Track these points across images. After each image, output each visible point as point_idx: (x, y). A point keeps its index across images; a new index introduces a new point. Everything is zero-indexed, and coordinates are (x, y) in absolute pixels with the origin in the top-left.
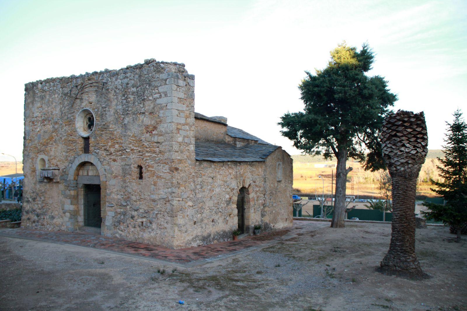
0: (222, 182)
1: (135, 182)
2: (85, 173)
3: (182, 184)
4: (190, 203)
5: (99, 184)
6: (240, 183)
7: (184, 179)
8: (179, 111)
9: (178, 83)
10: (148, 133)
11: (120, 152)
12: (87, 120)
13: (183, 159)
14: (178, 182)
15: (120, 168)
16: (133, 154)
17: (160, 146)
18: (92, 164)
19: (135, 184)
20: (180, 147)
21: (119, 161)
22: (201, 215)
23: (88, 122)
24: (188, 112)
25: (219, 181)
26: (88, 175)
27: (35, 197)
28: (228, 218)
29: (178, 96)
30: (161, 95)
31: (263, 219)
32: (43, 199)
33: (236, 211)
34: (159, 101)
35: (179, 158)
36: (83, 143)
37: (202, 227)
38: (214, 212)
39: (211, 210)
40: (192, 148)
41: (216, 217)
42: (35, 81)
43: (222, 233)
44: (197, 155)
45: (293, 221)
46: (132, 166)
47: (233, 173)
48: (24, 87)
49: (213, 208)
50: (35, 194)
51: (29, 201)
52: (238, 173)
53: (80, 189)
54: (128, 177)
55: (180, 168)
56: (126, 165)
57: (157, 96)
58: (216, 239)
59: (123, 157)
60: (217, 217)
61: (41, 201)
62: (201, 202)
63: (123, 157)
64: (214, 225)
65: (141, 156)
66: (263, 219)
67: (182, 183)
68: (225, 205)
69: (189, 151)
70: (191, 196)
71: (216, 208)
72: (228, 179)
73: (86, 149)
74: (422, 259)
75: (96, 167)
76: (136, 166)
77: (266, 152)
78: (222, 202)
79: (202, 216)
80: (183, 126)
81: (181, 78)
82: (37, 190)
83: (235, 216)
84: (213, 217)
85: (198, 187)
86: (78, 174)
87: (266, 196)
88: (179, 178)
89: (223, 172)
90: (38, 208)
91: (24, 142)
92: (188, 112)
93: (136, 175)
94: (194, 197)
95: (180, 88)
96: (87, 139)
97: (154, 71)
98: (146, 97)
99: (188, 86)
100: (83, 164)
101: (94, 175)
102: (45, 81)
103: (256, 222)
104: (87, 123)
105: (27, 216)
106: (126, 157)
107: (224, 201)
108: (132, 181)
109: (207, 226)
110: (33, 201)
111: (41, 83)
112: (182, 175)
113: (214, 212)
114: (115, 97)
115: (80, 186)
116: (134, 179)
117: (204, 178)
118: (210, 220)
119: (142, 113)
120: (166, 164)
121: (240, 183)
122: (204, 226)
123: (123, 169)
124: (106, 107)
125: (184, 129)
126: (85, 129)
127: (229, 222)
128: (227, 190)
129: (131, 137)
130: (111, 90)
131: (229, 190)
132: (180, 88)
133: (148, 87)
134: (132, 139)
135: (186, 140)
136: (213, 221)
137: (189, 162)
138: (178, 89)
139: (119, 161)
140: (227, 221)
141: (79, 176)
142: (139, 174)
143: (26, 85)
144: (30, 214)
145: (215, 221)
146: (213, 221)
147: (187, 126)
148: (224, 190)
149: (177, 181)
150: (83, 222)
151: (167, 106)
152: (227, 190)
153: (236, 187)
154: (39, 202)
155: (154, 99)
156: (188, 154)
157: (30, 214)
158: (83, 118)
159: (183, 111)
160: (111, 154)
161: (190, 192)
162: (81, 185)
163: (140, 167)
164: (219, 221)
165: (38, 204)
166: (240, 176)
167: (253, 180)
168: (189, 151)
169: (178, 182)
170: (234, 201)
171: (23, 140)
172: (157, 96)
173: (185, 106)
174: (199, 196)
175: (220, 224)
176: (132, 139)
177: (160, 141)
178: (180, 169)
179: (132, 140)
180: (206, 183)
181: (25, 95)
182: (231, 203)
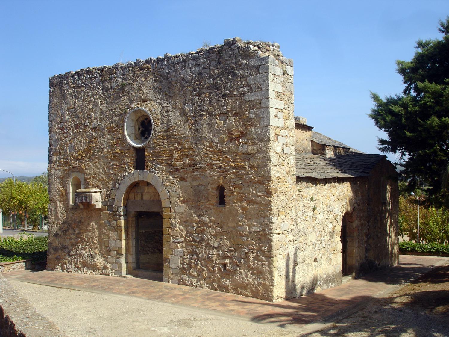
0: (325, 207)
1: (214, 209)
2: (139, 197)
3: (282, 211)
4: (291, 237)
5: (159, 211)
6: (344, 208)
7: (284, 204)
8: (277, 110)
9: (274, 71)
10: (233, 141)
11: (191, 168)
12: (140, 124)
13: (282, 176)
14: (277, 208)
15: (191, 189)
16: (211, 171)
17: (251, 158)
18: (148, 184)
19: (213, 211)
20: (279, 159)
21: (189, 179)
22: (302, 252)
23: (140, 127)
24: (286, 111)
25: (321, 205)
26: (142, 199)
27: (66, 229)
28: (331, 255)
29: (275, 90)
30: (251, 89)
31: (367, 255)
32: (77, 231)
33: (340, 246)
34: (248, 97)
35: (278, 175)
36: (135, 156)
37: (304, 270)
38: (316, 248)
39: (313, 246)
40: (292, 160)
41: (318, 255)
42: (63, 73)
43: (325, 276)
44: (299, 169)
45: (401, 256)
46: (209, 186)
47: (337, 193)
48: (48, 82)
49: (316, 242)
50: (66, 225)
51: (58, 234)
52: (342, 194)
53: (130, 219)
54: (203, 201)
55: (280, 189)
56: (200, 185)
57: (245, 89)
58: (319, 286)
59: (195, 174)
60: (320, 255)
61: (75, 234)
62: (303, 235)
63: (195, 174)
64: (316, 266)
65: (223, 173)
66: (367, 255)
67: (282, 210)
68: (329, 238)
69: (288, 165)
70: (292, 227)
71: (319, 242)
72: (332, 202)
73: (140, 164)
74: (127, 263)
75: (155, 188)
76: (215, 186)
77: (368, 164)
78: (325, 235)
79: (304, 254)
80: (282, 131)
81: (278, 64)
82: (68, 220)
83: (338, 253)
84: (315, 256)
85: (300, 214)
86: (128, 198)
87: (370, 224)
88: (279, 202)
89: (326, 192)
90: (70, 244)
91: (49, 156)
92: (286, 111)
93: (215, 200)
94: (296, 228)
95: (277, 77)
96: (140, 152)
97: (240, 55)
98: (228, 92)
99: (286, 75)
100: (135, 186)
101: (152, 199)
102: (77, 73)
103: (360, 260)
104: (139, 129)
105: (55, 254)
106: (200, 175)
107: (327, 233)
108: (209, 208)
109: (309, 268)
110: (64, 235)
111: (72, 76)
112: (282, 198)
113: (316, 248)
114: (182, 92)
115: (132, 214)
116: (211, 205)
117: (306, 201)
118: (312, 260)
119: (223, 114)
120: (261, 184)
121: (344, 208)
122: (305, 267)
123: (194, 190)
124: (169, 107)
125: (283, 135)
126: (138, 136)
127: (332, 260)
128: (330, 217)
129: (207, 147)
130: (176, 84)
131: (333, 217)
132: (277, 77)
133: (231, 78)
134: (208, 149)
135: (286, 150)
136: (316, 260)
137: (289, 180)
138: (275, 79)
139: (189, 179)
140: (331, 259)
141: (130, 201)
142: (219, 197)
143: (51, 80)
144: (60, 251)
145: (318, 260)
146: (316, 260)
147: (286, 131)
148: (327, 217)
149: (277, 206)
150: (134, 263)
151: (260, 103)
152: (330, 217)
153: (340, 213)
154: (72, 236)
155: (241, 94)
156: (287, 169)
157: (60, 251)
158: (134, 122)
159: (281, 110)
160: (177, 170)
161: (290, 222)
162: (133, 213)
163: (221, 189)
164: (322, 260)
165: (70, 239)
166: (344, 197)
167: (357, 202)
168: (288, 165)
169: (277, 208)
170: (338, 232)
171: (48, 153)
172: (245, 89)
173: (283, 102)
174: (300, 227)
175: (323, 265)
176: (208, 149)
177: (252, 152)
178: (279, 189)
179: (208, 150)
180: (308, 208)
181: (50, 92)
182: (335, 235)
